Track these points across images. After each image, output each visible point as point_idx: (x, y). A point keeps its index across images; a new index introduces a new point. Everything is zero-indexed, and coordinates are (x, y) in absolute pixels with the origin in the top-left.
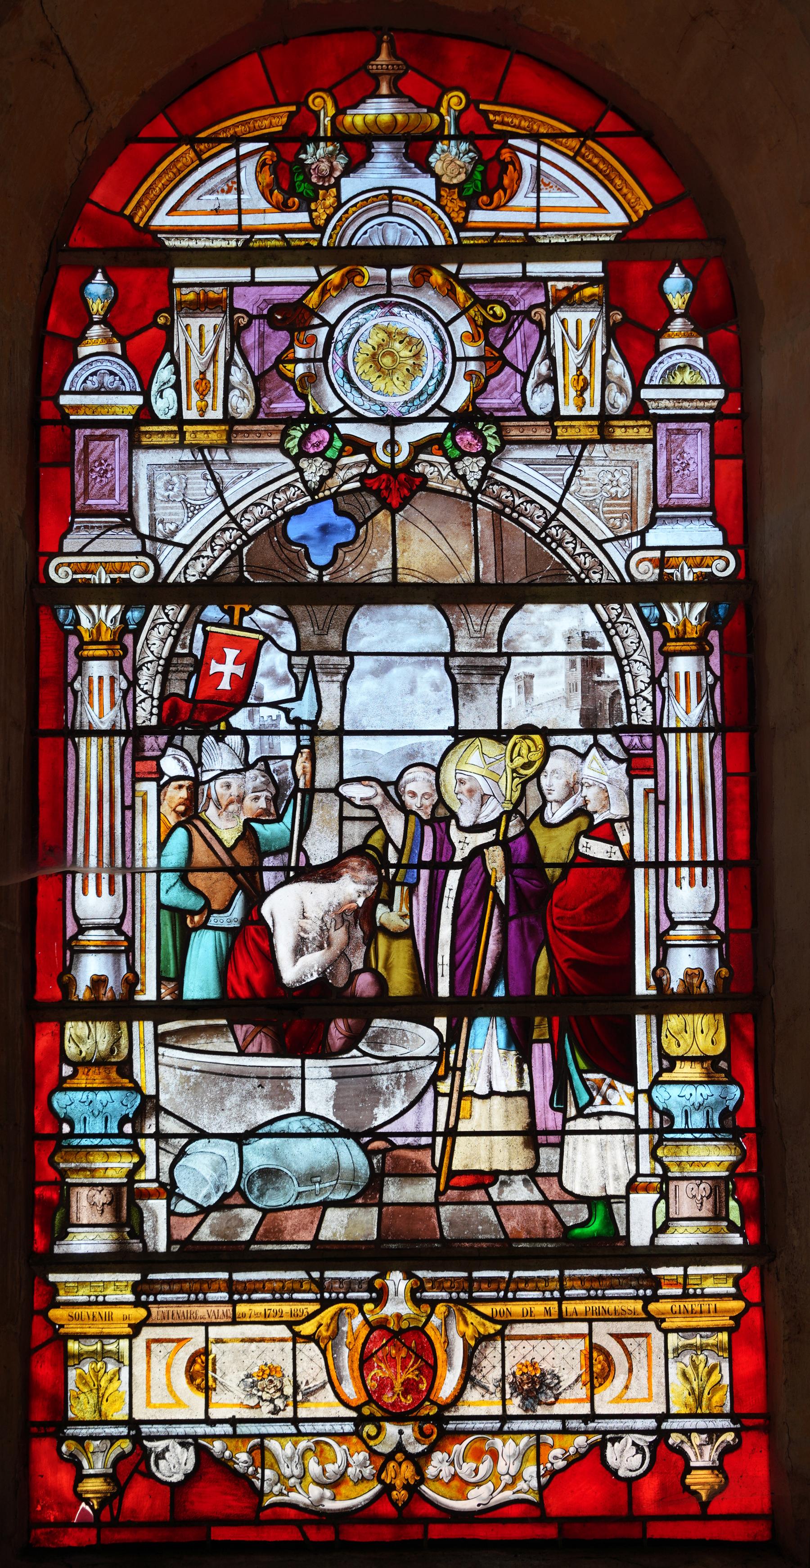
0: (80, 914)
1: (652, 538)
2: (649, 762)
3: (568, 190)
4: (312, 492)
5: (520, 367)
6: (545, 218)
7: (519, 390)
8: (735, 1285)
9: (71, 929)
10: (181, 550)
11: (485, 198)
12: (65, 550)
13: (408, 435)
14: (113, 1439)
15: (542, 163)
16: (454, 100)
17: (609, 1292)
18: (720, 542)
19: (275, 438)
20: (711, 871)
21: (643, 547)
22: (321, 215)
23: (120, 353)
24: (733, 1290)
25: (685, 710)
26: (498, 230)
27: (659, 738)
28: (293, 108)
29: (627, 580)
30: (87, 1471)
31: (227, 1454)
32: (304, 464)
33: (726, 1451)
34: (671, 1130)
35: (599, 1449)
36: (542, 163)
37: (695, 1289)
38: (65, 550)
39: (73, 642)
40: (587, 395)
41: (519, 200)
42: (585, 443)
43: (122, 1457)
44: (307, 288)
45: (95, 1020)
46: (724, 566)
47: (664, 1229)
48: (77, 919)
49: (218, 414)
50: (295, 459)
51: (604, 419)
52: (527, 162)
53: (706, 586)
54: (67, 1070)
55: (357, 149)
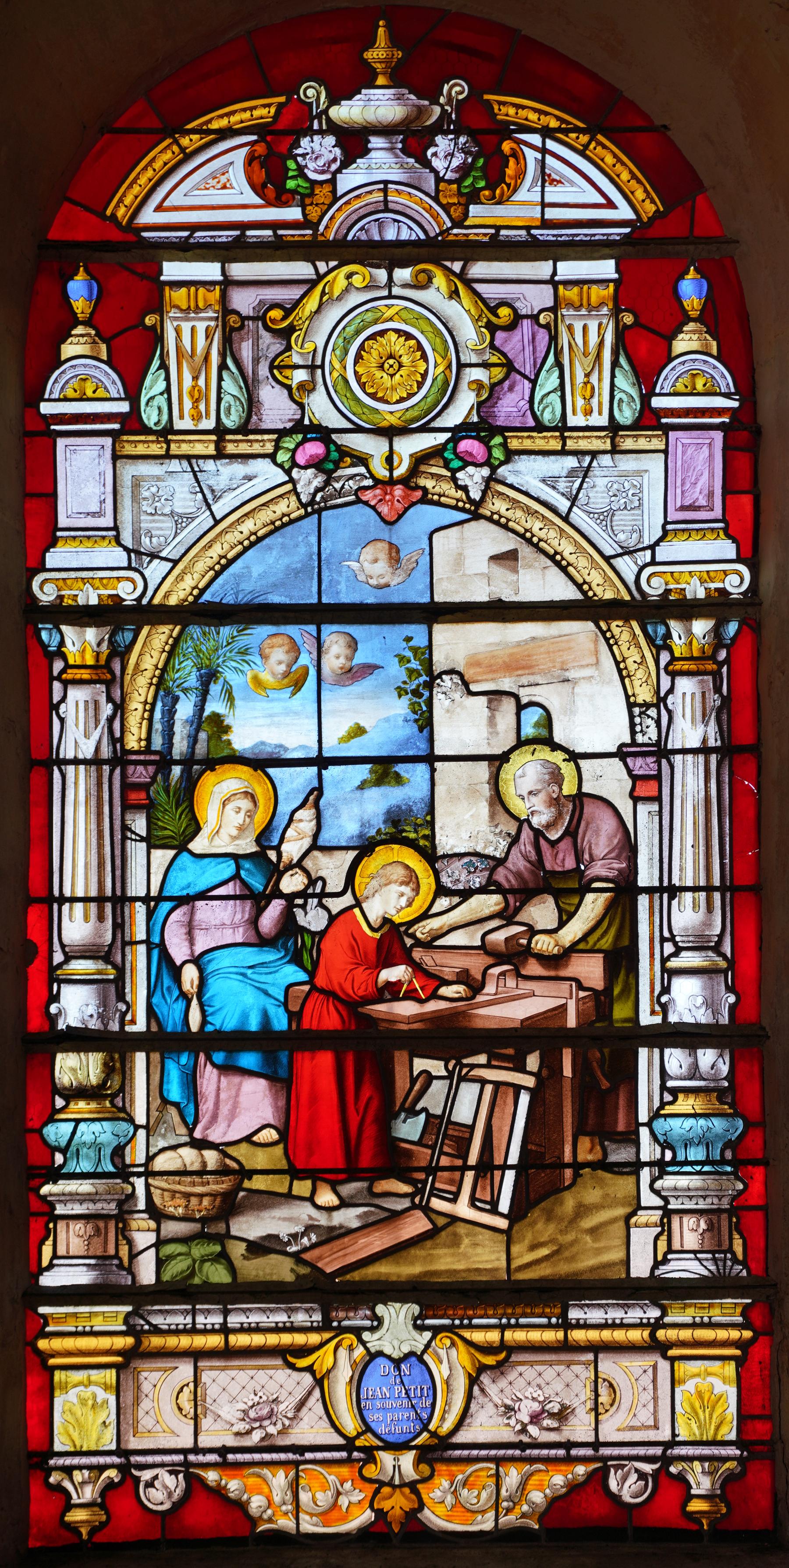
0: (66, 941)
1: (663, 553)
2: (654, 784)
3: (572, 183)
4: (304, 506)
5: (527, 373)
6: (551, 214)
7: (527, 398)
8: (742, 1314)
9: (58, 957)
10: (170, 565)
11: (487, 193)
12: (48, 566)
13: (408, 447)
14: (102, 1468)
15: (547, 156)
16: (457, 89)
17: (522, 1321)
18: (733, 556)
19: (269, 448)
20: (717, 896)
21: (653, 562)
22: (314, 213)
23: (105, 358)
24: (740, 1319)
25: (688, 732)
26: (498, 228)
27: (664, 762)
28: (282, 99)
29: (637, 596)
30: (75, 1500)
31: (548, 1491)
32: (295, 473)
33: (729, 1480)
34: (674, 1162)
35: (599, 1477)
36: (547, 156)
37: (702, 1318)
38: (48, 566)
39: (58, 666)
40: (595, 402)
41: (522, 195)
42: (594, 454)
43: (110, 1486)
44: (305, 288)
45: (87, 1051)
46: (737, 581)
47: (666, 1261)
48: (63, 946)
49: (603, 421)
50: (288, 472)
51: (614, 428)
52: (531, 156)
53: (717, 605)
54: (59, 1102)
55: (354, 142)
